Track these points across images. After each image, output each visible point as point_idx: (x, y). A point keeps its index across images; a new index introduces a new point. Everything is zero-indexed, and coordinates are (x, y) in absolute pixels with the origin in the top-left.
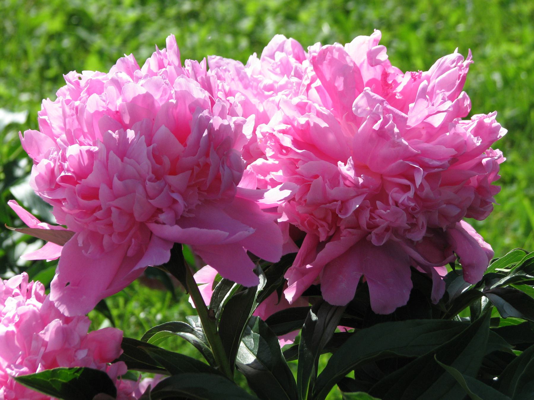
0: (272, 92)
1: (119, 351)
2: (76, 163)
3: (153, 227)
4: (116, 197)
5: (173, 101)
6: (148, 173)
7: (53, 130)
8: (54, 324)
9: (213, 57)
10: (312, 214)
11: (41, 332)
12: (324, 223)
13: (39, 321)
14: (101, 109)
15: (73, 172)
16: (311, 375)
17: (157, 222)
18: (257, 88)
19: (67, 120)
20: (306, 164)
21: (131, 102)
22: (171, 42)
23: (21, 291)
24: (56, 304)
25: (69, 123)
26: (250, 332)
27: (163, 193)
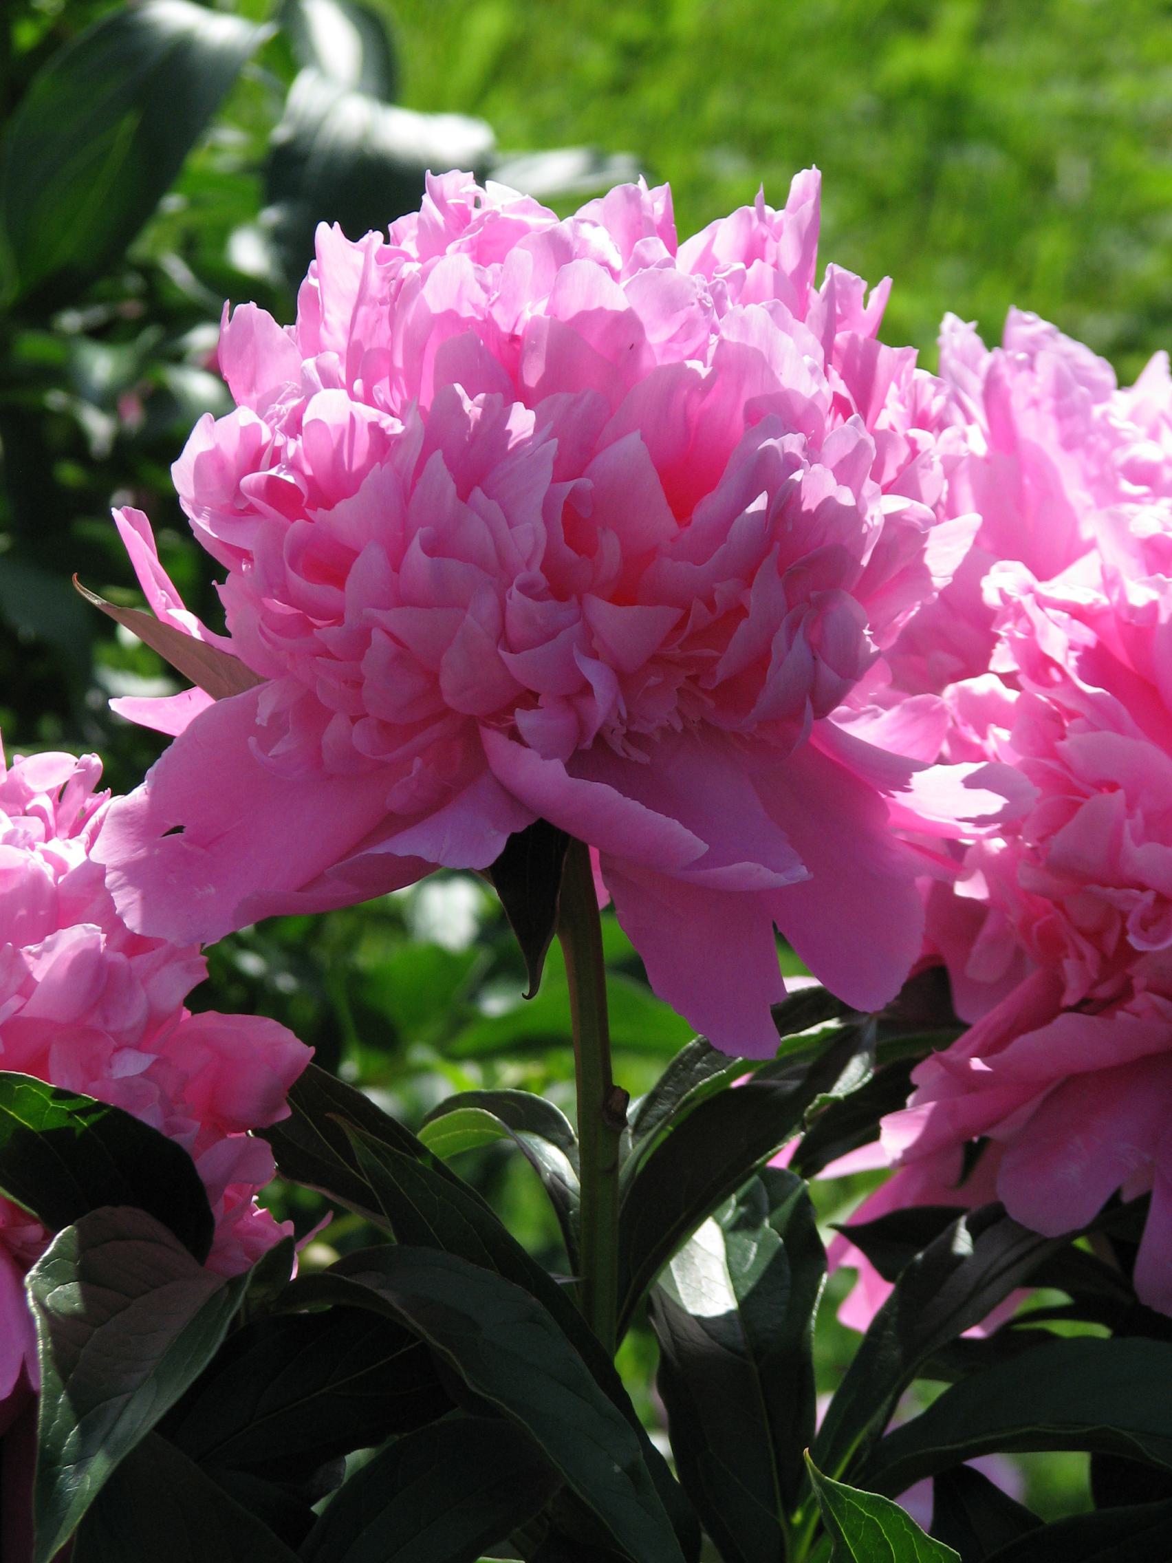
0: (1143, 489)
1: (275, 1108)
2: (325, 452)
3: (495, 741)
4: (401, 600)
5: (701, 369)
6: (528, 564)
7: (322, 330)
8: (77, 937)
9: (1030, 317)
10: (1059, 905)
11: (30, 947)
12: (1087, 949)
13: (42, 913)
14: (467, 312)
15: (310, 481)
16: (872, 1424)
17: (514, 735)
18: (1103, 459)
19: (363, 310)
20: (1092, 735)
21: (571, 322)
22: (805, 193)
23: (56, 808)
24: (108, 879)
25: (366, 322)
26: (761, 1220)
27: (549, 646)
